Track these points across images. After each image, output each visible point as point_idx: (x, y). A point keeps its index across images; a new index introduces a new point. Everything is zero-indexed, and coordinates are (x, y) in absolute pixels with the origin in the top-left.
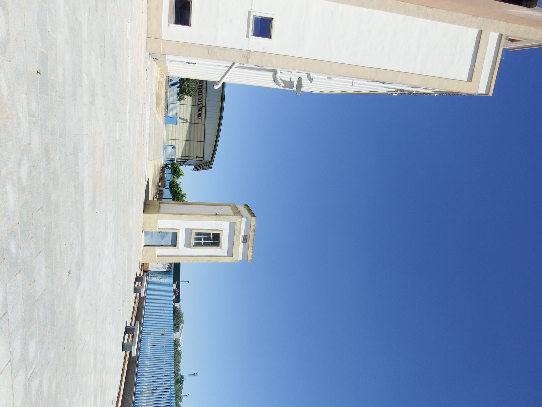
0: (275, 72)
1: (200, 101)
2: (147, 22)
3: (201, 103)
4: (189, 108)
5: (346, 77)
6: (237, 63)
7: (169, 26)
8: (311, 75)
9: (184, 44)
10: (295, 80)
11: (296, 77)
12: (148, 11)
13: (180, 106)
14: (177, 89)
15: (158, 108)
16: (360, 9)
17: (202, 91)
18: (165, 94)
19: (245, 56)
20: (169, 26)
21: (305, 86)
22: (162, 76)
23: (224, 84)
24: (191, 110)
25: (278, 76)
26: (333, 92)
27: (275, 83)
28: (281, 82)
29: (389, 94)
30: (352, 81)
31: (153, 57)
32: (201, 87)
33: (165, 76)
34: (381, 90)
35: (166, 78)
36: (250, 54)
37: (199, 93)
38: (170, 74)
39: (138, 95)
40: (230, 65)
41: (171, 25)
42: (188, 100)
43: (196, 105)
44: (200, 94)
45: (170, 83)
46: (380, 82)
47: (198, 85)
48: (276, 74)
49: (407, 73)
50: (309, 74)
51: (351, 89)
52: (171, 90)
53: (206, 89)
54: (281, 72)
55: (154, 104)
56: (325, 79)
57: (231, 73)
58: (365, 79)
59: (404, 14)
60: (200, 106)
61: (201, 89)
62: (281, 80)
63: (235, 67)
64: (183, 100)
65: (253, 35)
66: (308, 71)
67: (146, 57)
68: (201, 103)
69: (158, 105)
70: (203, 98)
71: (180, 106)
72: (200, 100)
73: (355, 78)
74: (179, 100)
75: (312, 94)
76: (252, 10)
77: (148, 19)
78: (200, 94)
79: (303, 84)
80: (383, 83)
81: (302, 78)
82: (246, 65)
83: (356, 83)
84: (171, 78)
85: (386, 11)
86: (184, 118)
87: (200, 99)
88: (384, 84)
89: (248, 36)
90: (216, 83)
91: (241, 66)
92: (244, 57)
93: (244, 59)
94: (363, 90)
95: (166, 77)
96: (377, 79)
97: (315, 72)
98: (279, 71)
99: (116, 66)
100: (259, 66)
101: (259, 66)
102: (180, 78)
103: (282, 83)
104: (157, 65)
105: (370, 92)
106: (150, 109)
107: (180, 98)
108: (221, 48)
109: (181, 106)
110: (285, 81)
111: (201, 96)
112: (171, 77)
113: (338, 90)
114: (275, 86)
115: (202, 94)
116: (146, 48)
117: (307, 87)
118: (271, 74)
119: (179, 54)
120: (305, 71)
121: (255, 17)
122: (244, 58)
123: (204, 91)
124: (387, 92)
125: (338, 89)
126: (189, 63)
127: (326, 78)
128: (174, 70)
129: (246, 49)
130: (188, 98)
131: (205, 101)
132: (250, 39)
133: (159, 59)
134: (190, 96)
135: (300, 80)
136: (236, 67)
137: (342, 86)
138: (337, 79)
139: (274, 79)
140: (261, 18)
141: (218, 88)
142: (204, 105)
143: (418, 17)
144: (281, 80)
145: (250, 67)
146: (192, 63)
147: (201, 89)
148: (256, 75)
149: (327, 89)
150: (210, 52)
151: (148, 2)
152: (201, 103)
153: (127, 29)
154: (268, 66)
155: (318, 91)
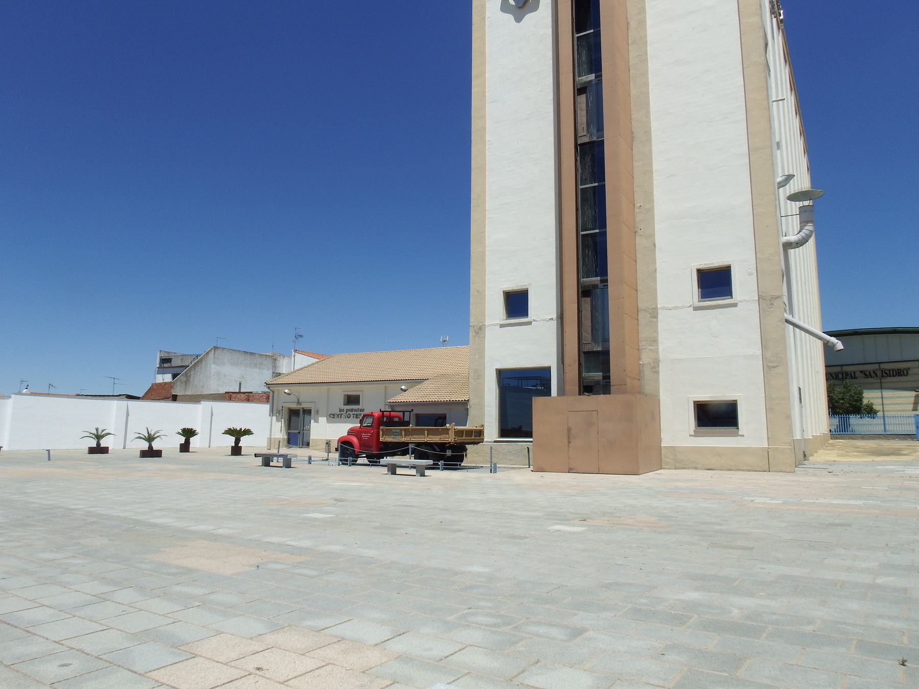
0: (788, 246)
1: (868, 373)
2: (743, 471)
3: (874, 372)
4: (887, 393)
5: (770, 116)
6: (785, 315)
7: (743, 436)
8: (779, 179)
9: (769, 410)
10: (795, 206)
11: (789, 206)
12: (725, 470)
13: (888, 411)
14: (854, 420)
15: (904, 452)
16: (653, 139)
17: (847, 374)
18: (867, 439)
19: (770, 302)
20: (743, 436)
21: (804, 185)
22: (832, 445)
23: (831, 334)
24: (893, 391)
25: (793, 238)
26: (800, 131)
27: (809, 241)
28: (803, 231)
29: (783, 27)
30: (775, 103)
31: (801, 462)
32: (840, 376)
33: (831, 441)
34: (778, 44)
35: (834, 439)
36: (764, 295)
37: (852, 378)
38: (826, 433)
39: (886, 488)
40: (791, 327)
41: (740, 433)
42: (870, 396)
43: (879, 381)
44: (853, 376)
45: (841, 432)
46: (766, 52)
47: (835, 382)
48: (790, 243)
49: (739, 11)
50: (779, 183)
51: (790, 101)
52: (856, 428)
53: (841, 366)
54: (786, 236)
55: (896, 459)
56: (781, 152)
57: (804, 322)
58: (767, 81)
59: (646, 60)
60: (879, 373)
61: (843, 376)
62: (798, 233)
63: (793, 317)
64: (874, 407)
65: (730, 297)
66: (775, 186)
67: (806, 472)
68: (874, 372)
69: (896, 452)
70: (862, 370)
71: (888, 411)
72: (867, 375)
73: (768, 99)
74: (876, 414)
75: (813, 168)
76: (691, 306)
77: (739, 470)
78: (853, 376)
79: (802, 188)
80: (766, 45)
81: (788, 195)
82: (786, 300)
83: (777, 96)
84: (833, 430)
85: (648, 93)
86: (913, 401)
87: (866, 375)
88: (767, 44)
89: (735, 305)
90: (828, 347)
91: (788, 307)
92: (771, 304)
93: (775, 304)
94: (786, 78)
95: (832, 439)
96: (763, 58)
97: (773, 173)
98: (785, 239)
99: (838, 525)
100: (783, 275)
101: (783, 275)
102: (829, 415)
103: (806, 228)
104: (815, 455)
105: (788, 63)
106: (908, 466)
107: (870, 411)
108: (764, 347)
109: (888, 409)
110: (800, 223)
111: (858, 374)
112: (830, 430)
113: (795, 123)
114: (812, 241)
115: (854, 373)
116: (788, 472)
117: (802, 182)
118: (792, 252)
119: (789, 417)
120: (775, 193)
121: (702, 298)
122: (774, 305)
123: (845, 369)
124: (780, 31)
125: (794, 123)
126: (800, 400)
127: (779, 152)
128: (817, 425)
129: (757, 304)
130: (868, 398)
131: (834, 367)
132: (739, 299)
133: (804, 452)
134: (861, 393)
135: (793, 198)
136: (791, 316)
137: (787, 119)
138: (777, 131)
139: (801, 246)
140: (701, 289)
141: (840, 342)
142: (877, 366)
143: (645, 36)
144: (798, 233)
145: (786, 292)
146: (800, 394)
147: (843, 376)
148: (799, 279)
149: (798, 144)
150: (775, 364)
151: (712, 469)
152: (872, 373)
153: (765, 503)
154: (780, 259)
155: (804, 161)
